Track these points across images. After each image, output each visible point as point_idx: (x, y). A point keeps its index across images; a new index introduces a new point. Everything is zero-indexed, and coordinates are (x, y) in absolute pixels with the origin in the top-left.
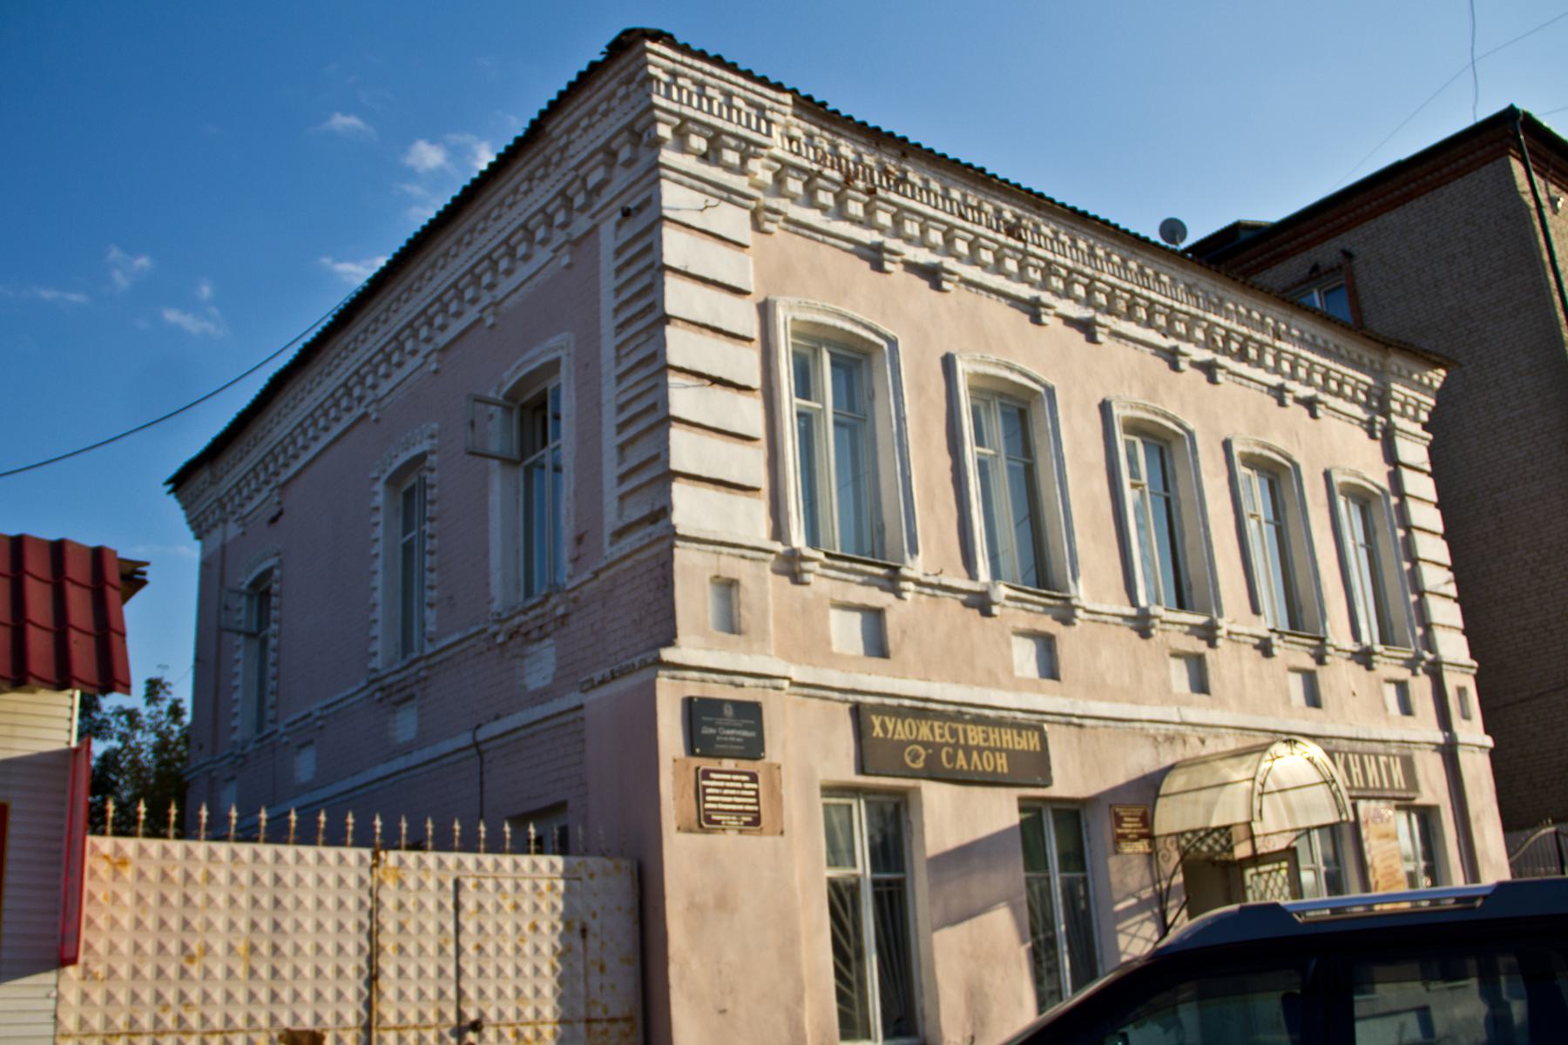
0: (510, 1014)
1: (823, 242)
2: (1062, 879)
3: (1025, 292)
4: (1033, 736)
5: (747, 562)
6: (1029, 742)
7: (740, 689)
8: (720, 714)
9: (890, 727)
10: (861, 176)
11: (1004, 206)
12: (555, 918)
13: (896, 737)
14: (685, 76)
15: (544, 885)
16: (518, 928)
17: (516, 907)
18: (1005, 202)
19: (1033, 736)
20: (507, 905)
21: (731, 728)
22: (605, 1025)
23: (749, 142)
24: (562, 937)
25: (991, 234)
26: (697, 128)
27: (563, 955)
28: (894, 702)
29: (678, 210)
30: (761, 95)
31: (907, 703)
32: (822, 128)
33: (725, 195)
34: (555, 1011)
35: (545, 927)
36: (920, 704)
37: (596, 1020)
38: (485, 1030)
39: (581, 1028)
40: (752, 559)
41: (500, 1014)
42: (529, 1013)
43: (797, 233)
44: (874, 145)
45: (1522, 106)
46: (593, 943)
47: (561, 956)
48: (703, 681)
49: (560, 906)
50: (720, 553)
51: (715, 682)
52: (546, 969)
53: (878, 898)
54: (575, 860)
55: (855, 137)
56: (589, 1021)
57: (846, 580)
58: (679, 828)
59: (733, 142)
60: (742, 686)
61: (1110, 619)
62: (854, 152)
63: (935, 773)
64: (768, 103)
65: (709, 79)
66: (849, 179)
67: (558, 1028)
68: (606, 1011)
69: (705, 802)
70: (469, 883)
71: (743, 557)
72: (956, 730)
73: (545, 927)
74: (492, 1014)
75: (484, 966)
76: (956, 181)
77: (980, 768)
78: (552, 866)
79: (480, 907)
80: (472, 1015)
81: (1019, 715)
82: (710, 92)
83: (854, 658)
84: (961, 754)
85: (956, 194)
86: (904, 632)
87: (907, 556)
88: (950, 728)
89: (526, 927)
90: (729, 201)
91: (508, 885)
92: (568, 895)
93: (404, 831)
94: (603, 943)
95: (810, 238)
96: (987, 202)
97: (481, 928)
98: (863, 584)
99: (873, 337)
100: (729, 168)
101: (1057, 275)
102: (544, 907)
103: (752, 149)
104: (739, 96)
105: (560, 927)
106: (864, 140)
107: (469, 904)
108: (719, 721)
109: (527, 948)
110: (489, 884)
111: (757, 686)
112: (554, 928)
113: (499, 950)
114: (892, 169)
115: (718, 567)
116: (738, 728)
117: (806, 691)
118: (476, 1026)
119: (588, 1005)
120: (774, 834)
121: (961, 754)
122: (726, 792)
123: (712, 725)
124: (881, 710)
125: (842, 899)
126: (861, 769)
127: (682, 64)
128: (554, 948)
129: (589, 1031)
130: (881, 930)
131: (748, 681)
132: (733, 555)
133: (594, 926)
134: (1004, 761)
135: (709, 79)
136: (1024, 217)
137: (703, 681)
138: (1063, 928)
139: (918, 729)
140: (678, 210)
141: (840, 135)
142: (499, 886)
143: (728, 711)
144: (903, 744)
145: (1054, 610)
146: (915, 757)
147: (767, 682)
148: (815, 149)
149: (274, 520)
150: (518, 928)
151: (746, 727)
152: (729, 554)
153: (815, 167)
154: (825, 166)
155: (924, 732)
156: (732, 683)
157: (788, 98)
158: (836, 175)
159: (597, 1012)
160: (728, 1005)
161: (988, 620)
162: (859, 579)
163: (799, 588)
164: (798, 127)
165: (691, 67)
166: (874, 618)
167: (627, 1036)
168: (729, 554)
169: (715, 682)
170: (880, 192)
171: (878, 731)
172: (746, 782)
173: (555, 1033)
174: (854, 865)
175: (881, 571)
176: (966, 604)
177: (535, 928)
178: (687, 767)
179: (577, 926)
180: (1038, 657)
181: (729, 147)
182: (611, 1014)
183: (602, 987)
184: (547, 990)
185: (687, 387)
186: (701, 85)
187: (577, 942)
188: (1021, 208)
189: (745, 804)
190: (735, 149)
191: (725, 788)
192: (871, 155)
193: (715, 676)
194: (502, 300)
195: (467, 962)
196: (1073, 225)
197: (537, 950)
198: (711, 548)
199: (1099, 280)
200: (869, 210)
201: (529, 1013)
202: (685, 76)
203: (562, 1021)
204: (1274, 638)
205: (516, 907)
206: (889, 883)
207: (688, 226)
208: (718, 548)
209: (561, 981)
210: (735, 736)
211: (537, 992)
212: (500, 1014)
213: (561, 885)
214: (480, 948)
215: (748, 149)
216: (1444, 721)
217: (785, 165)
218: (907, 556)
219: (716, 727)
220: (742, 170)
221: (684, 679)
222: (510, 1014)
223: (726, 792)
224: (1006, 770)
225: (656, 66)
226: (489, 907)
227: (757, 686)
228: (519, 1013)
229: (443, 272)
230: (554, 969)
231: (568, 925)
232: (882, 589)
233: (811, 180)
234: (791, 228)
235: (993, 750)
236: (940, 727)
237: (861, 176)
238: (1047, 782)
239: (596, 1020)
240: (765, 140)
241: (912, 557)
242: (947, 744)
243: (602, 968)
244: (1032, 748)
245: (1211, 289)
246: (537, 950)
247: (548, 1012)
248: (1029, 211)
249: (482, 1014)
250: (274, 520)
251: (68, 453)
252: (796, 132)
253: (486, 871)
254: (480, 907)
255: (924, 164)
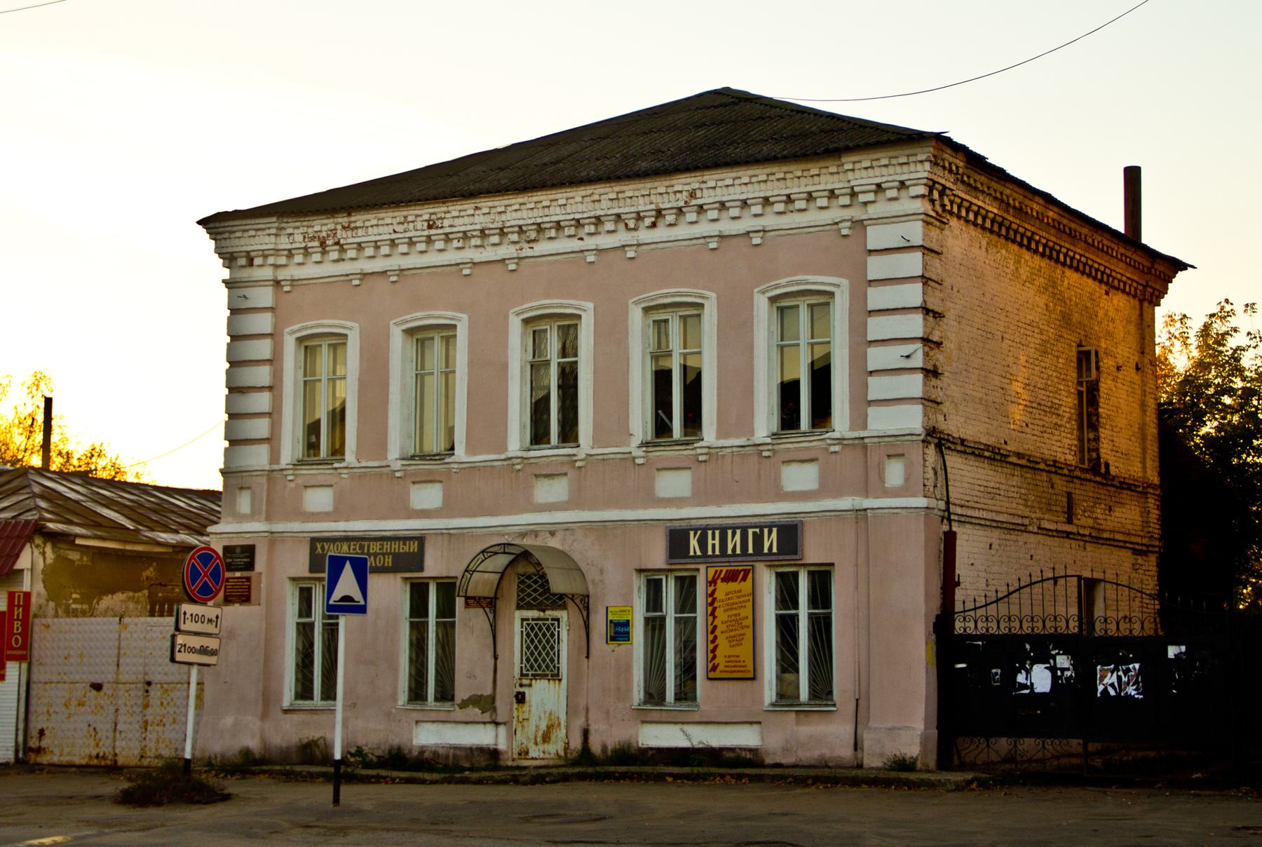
4: (414, 544)
9: (326, 547)
19: (414, 544)
25: (419, 233)
45: (213, 251)
72: (364, 546)
77: (374, 565)
88: (360, 545)
108: (234, 555)
126: (311, 571)
130: (327, 655)
134: (390, 560)
143: (238, 550)
149: (991, 545)
194: (769, 231)
224: (390, 564)
229: (732, 222)
235: (383, 555)
236: (354, 545)
238: (421, 569)
250: (991, 545)
251: (723, 515)
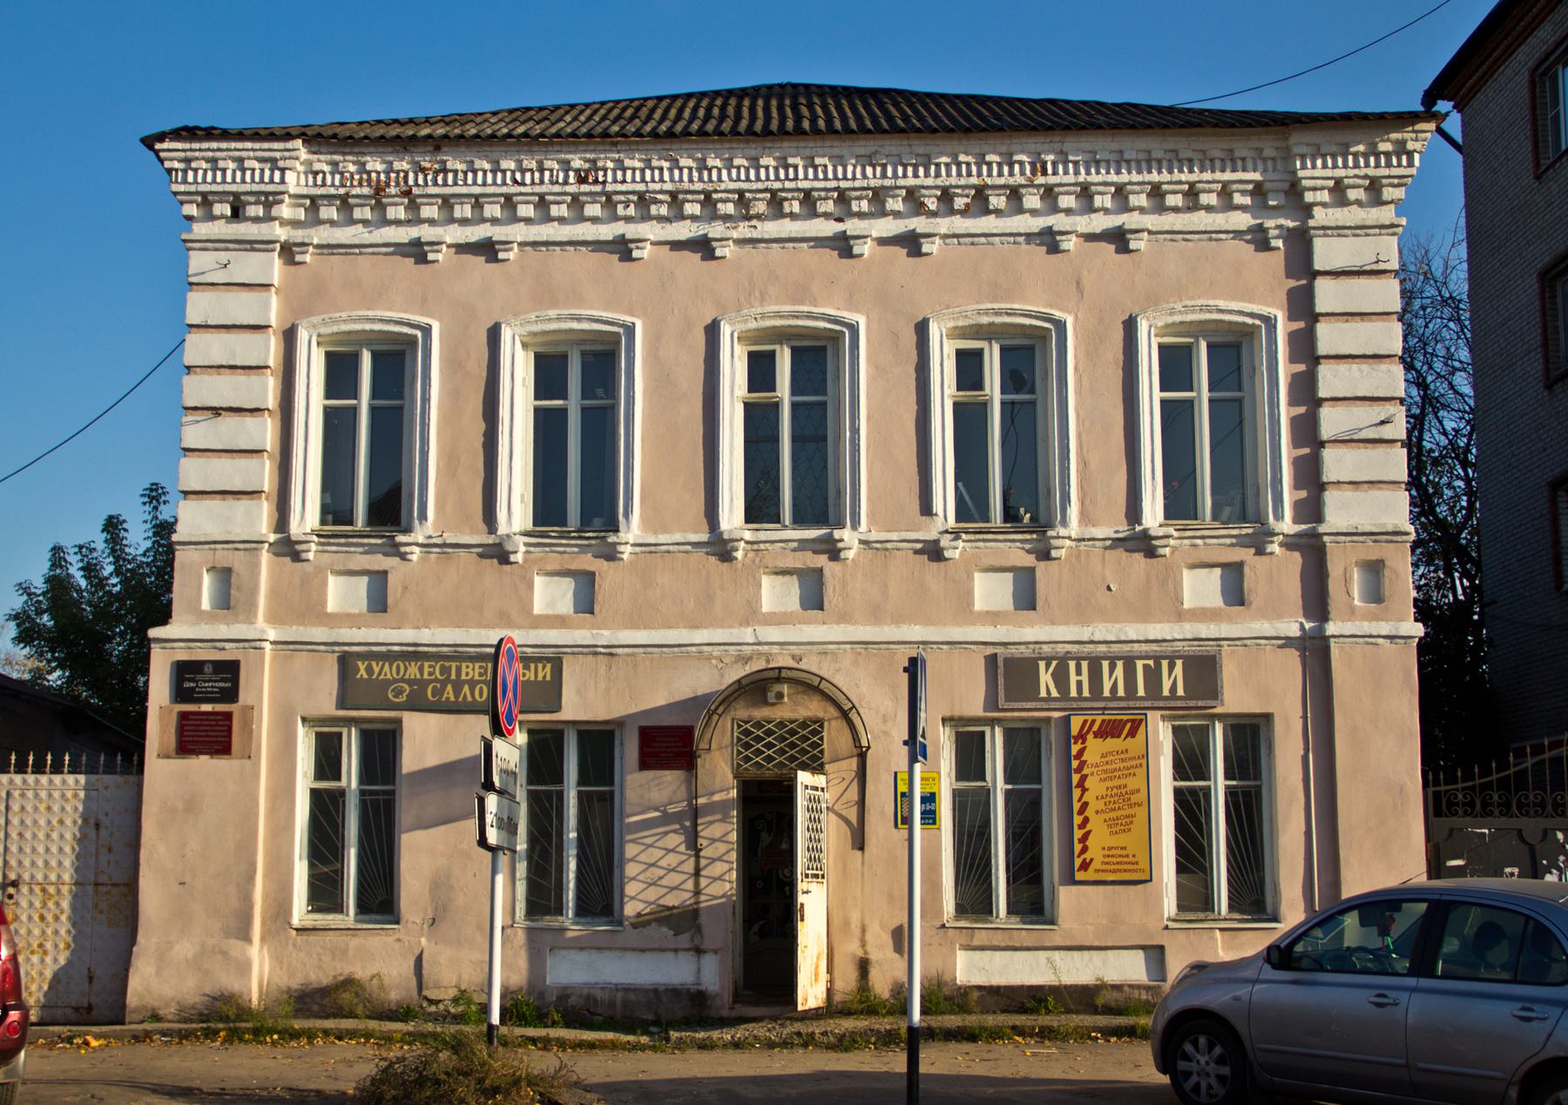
0: (40, 877)
1: (361, 254)
2: (580, 794)
3: (607, 232)
5: (242, 553)
6: (545, 672)
7: (223, 652)
8: (201, 672)
9: (377, 670)
10: (393, 184)
11: (569, 156)
12: (77, 816)
13: (382, 677)
14: (197, 159)
15: (69, 794)
16: (49, 822)
17: (49, 808)
18: (570, 152)
20: (42, 807)
21: (209, 681)
22: (109, 887)
23: (267, 194)
24: (81, 828)
26: (216, 198)
27: (81, 840)
28: (383, 649)
29: (203, 273)
30: (270, 150)
31: (396, 648)
32: (344, 154)
33: (248, 246)
34: (72, 876)
35: (68, 822)
36: (411, 649)
37: (102, 884)
38: (20, 887)
39: (90, 889)
40: (245, 550)
41: (33, 877)
42: (53, 877)
43: (333, 254)
44: (401, 149)
46: (104, 833)
47: (79, 841)
48: (189, 648)
49: (81, 808)
50: (215, 549)
51: (200, 648)
52: (68, 849)
53: (363, 805)
54: (94, 777)
55: (380, 150)
56: (97, 884)
57: (347, 552)
58: (159, 755)
59: (252, 199)
60: (224, 649)
61: (671, 548)
62: (384, 162)
63: (418, 704)
64: (278, 155)
65: (218, 154)
66: (379, 191)
67: (73, 887)
68: (111, 878)
69: (1080, 698)
70: (16, 794)
71: (237, 549)
73: (68, 822)
74: (26, 877)
75: (23, 846)
76: (506, 152)
77: (469, 698)
78: (77, 782)
79: (23, 808)
80: (13, 876)
81: (529, 650)
82: (221, 164)
83: (359, 615)
84: (449, 688)
85: (508, 164)
86: (405, 588)
87: (416, 522)
89: (55, 822)
90: (253, 250)
91: (43, 794)
92: (86, 801)
93: (13, 761)
94: (112, 833)
95: (346, 254)
96: (547, 159)
97: (22, 822)
98: (365, 553)
99: (406, 330)
100: (256, 220)
101: (656, 201)
102: (69, 808)
103: (271, 198)
104: (249, 158)
105: (80, 822)
106: (390, 149)
107: (16, 807)
108: (199, 677)
109: (55, 835)
110: (30, 794)
111: (237, 648)
112: (75, 822)
113: (35, 836)
114: (428, 165)
115: (214, 560)
116: (215, 681)
117: (292, 647)
118: (15, 884)
119: (96, 874)
120: (242, 757)
121: (449, 688)
122: (201, 728)
123: (191, 680)
124: (368, 656)
125: (326, 807)
127: (191, 150)
128: (74, 835)
129: (96, 892)
131: (228, 645)
132: (228, 549)
133: (105, 820)
135: (218, 154)
136: (600, 159)
137: (189, 648)
138: (573, 835)
139: (406, 669)
140: (203, 273)
141: (364, 154)
142: (37, 795)
143: (208, 669)
144: (388, 683)
145: (593, 549)
146: (398, 693)
147: (246, 645)
148: (342, 174)
150: (49, 822)
151: (223, 680)
152: (223, 549)
153: (342, 191)
154: (352, 186)
155: (413, 671)
156: (215, 648)
157: (298, 143)
158: (366, 191)
159: (103, 879)
160: (187, 880)
161: (507, 568)
162: (360, 549)
163: (299, 565)
164: (319, 161)
165: (200, 150)
166: (379, 580)
167: (125, 896)
168: (223, 549)
169: (200, 648)
170: (415, 191)
171: (363, 673)
172: (220, 720)
173: (71, 891)
174: (339, 779)
175: (379, 541)
176: (481, 556)
177: (61, 822)
178: (171, 711)
179: (92, 821)
180: (576, 594)
181: (250, 203)
182: (114, 881)
183: (109, 863)
184: (67, 863)
185: (198, 422)
186: (214, 161)
187: (92, 833)
188: (594, 151)
189: (217, 736)
190: (257, 203)
191: (214, 726)
192: (403, 160)
193: (199, 644)
195: (12, 844)
196: (668, 146)
197: (62, 836)
198: (207, 546)
199: (716, 191)
200: (413, 206)
201: (53, 877)
202: (197, 159)
203: (76, 884)
204: (945, 541)
205: (49, 808)
206: (1193, 791)
207: (213, 284)
208: (213, 546)
209: (78, 857)
210: (212, 687)
211: (60, 864)
212: (33, 877)
213: (82, 794)
214: (21, 835)
215: (270, 200)
216: (1317, 601)
217: (313, 199)
218: (416, 522)
219: (197, 682)
220: (269, 218)
221: (173, 648)
222: (40, 877)
223: (201, 728)
225: (171, 159)
226: (29, 808)
227: (237, 648)
228: (46, 877)
230: (73, 849)
231: (85, 820)
232: (385, 554)
233: (345, 203)
234: (325, 251)
237: (393, 184)
239: (102, 884)
240: (281, 188)
241: (421, 523)
242: (437, 680)
243: (110, 850)
244: (540, 678)
245: (905, 150)
246: (62, 836)
247: (66, 877)
248: (601, 152)
249: (19, 876)
252: (317, 166)
253: (29, 785)
254: (23, 808)
255: (463, 149)
